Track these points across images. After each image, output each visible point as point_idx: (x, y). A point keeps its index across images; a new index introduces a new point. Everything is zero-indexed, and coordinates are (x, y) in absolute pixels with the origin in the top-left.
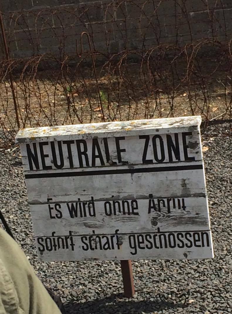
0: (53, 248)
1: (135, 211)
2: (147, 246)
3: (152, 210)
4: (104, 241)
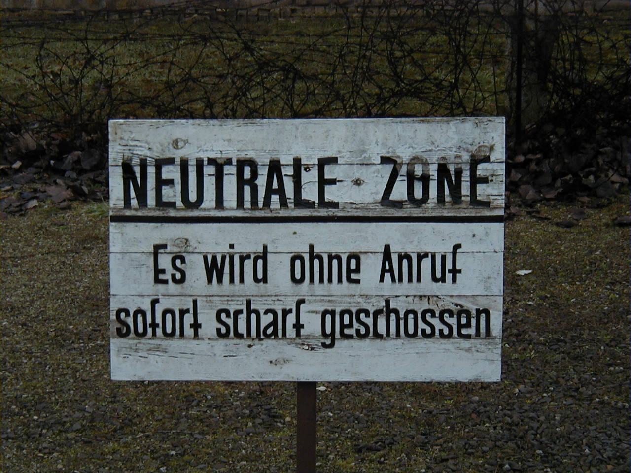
0: (150, 330)
1: (353, 276)
2: (358, 331)
3: (387, 276)
4: (266, 319)
